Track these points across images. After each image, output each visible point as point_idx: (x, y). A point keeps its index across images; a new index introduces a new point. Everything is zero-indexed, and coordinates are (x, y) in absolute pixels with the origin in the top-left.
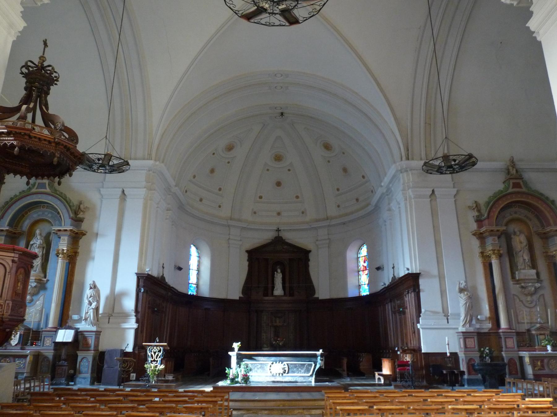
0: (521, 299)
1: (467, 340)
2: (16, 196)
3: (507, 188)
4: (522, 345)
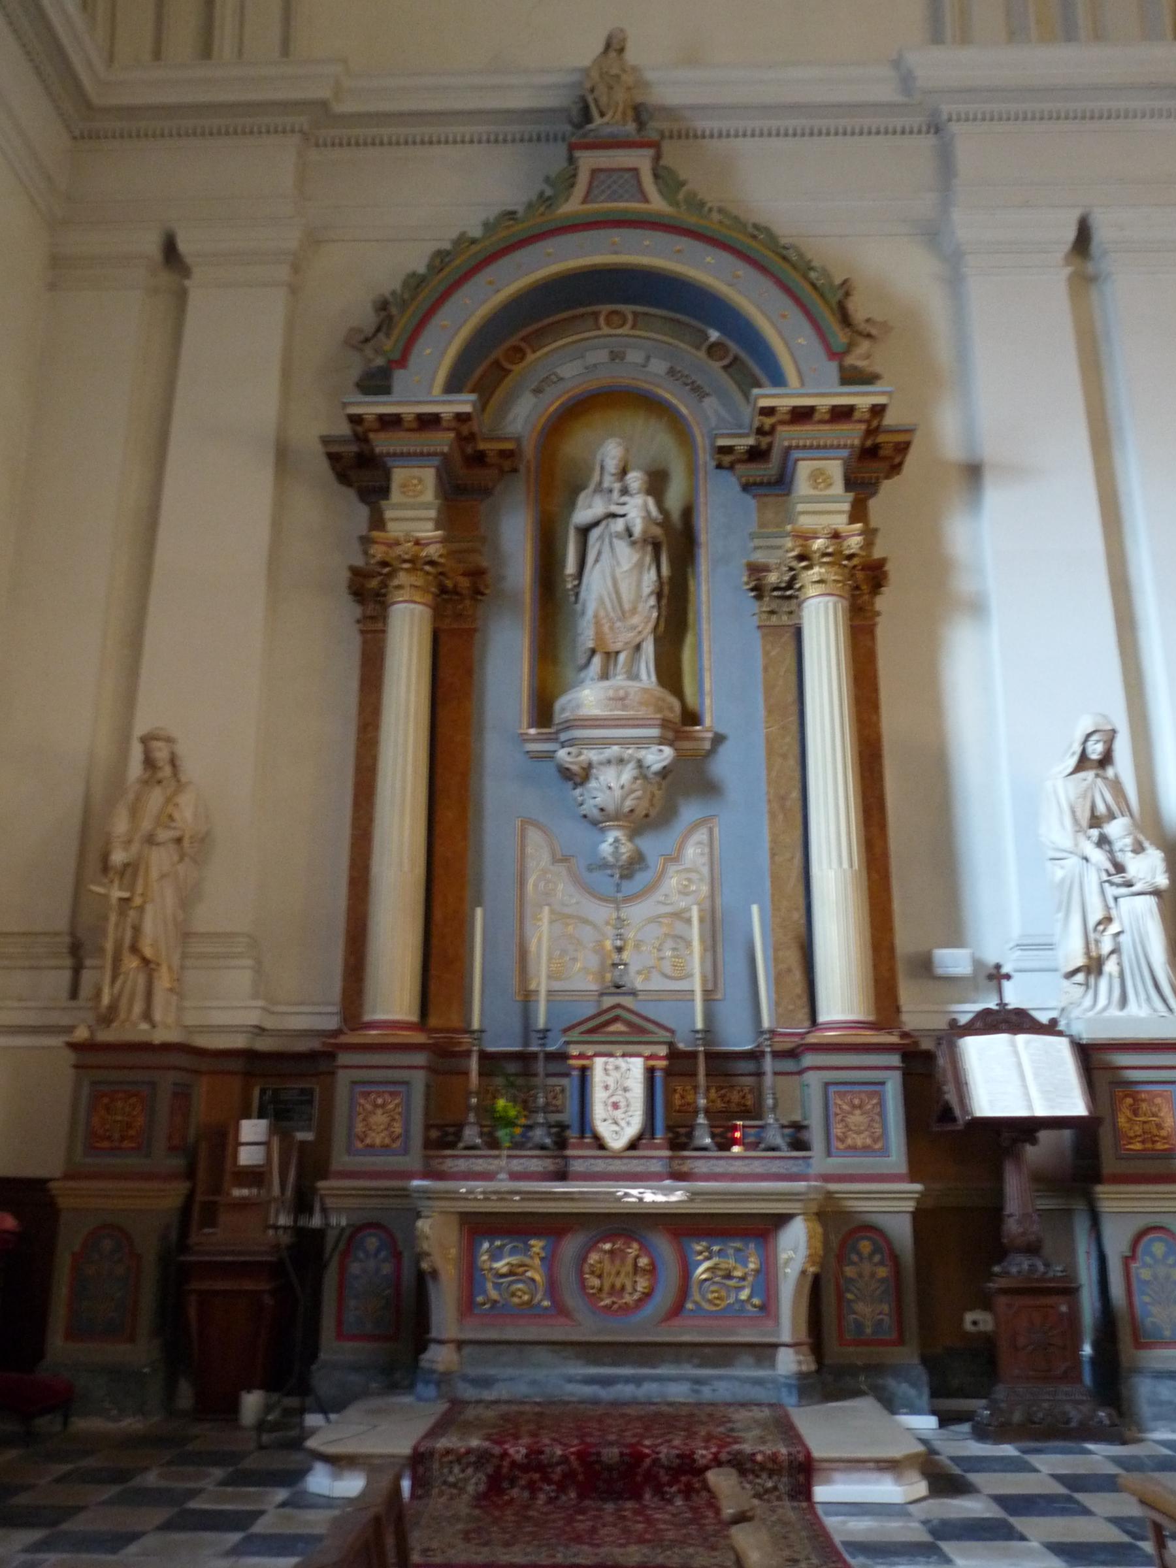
2: (464, 242)
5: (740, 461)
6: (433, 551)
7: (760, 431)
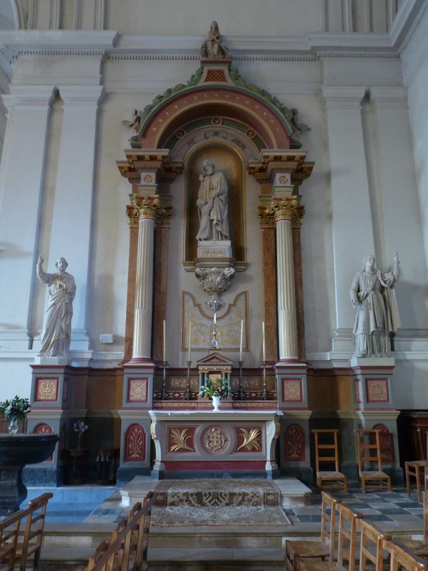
0: (198, 302)
1: (42, 383)
3: (194, 79)
4: (253, 395)
5: (257, 172)
6: (156, 202)
7: (264, 163)
